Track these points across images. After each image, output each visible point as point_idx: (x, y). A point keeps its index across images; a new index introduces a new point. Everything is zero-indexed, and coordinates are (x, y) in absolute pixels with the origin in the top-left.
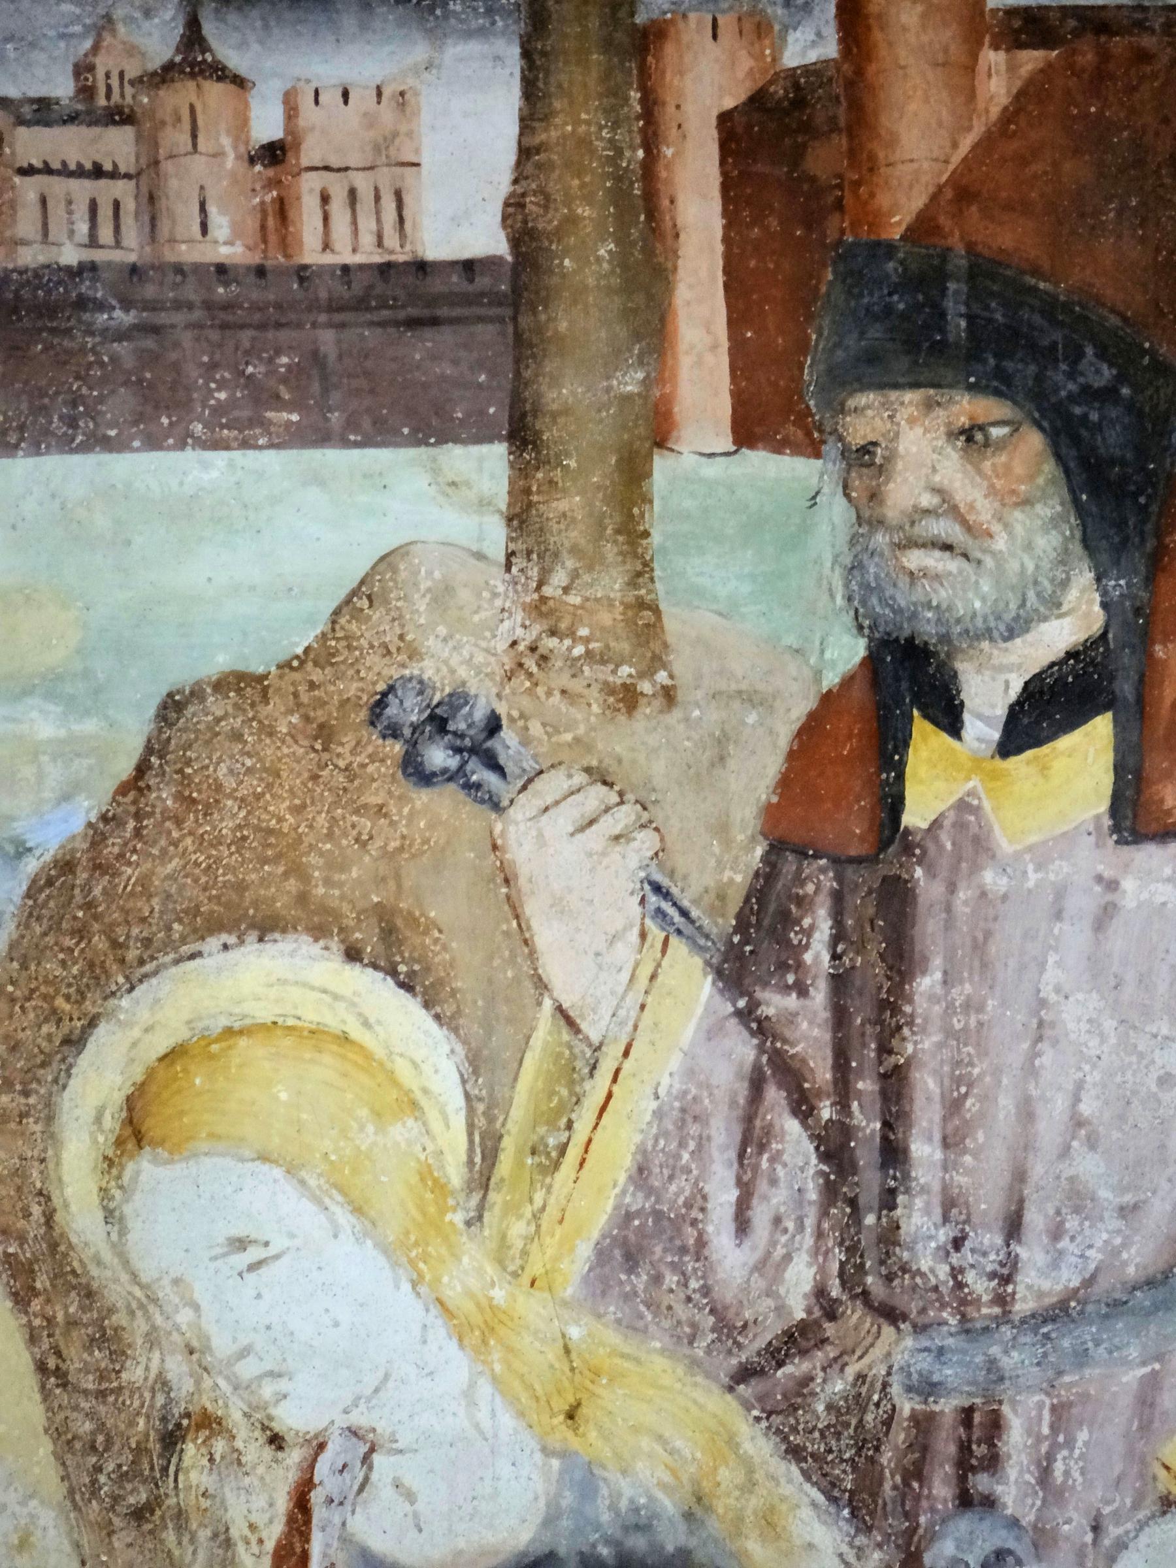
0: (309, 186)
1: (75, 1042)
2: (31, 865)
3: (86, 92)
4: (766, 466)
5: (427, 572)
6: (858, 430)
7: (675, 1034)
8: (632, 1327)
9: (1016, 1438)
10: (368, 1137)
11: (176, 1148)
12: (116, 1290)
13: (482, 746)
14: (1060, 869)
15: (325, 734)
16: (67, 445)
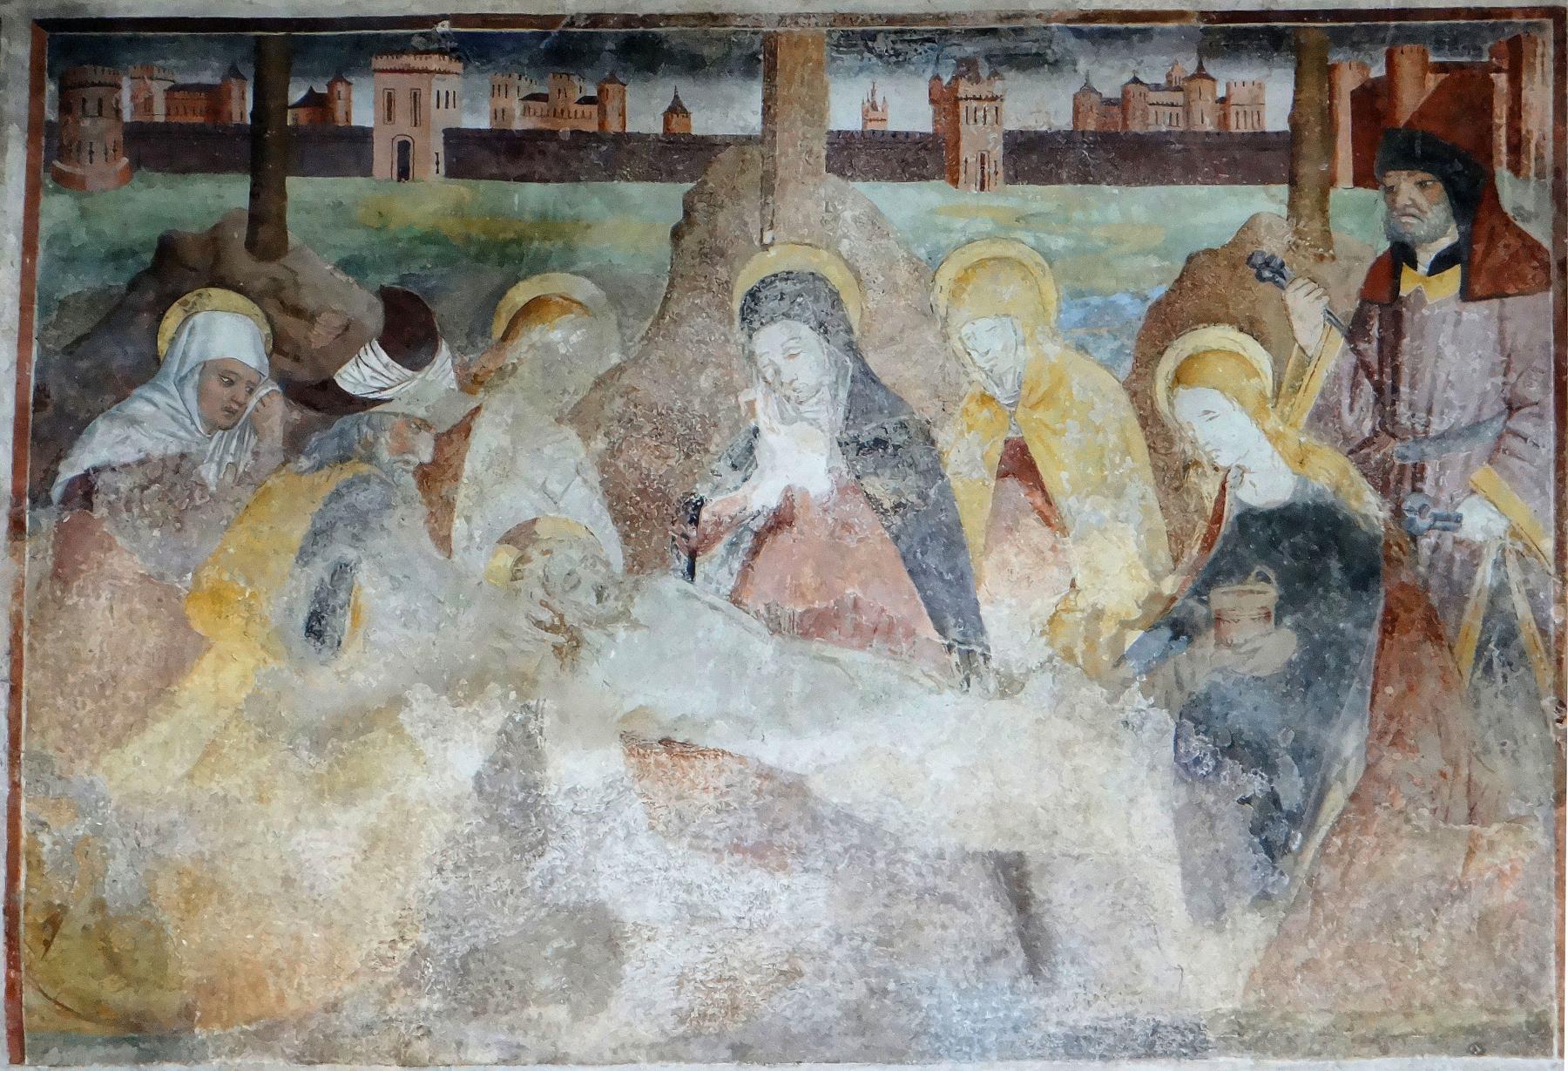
0: (1233, 110)
1: (1161, 354)
2: (1150, 303)
3: (1170, 82)
4: (1361, 192)
5: (1265, 221)
6: (1389, 182)
7: (1330, 354)
8: (1320, 438)
9: (1429, 472)
10: (1244, 382)
11: (1189, 384)
12: (1171, 425)
13: (1279, 271)
14: (1444, 310)
15: (1235, 267)
16: (1161, 183)
